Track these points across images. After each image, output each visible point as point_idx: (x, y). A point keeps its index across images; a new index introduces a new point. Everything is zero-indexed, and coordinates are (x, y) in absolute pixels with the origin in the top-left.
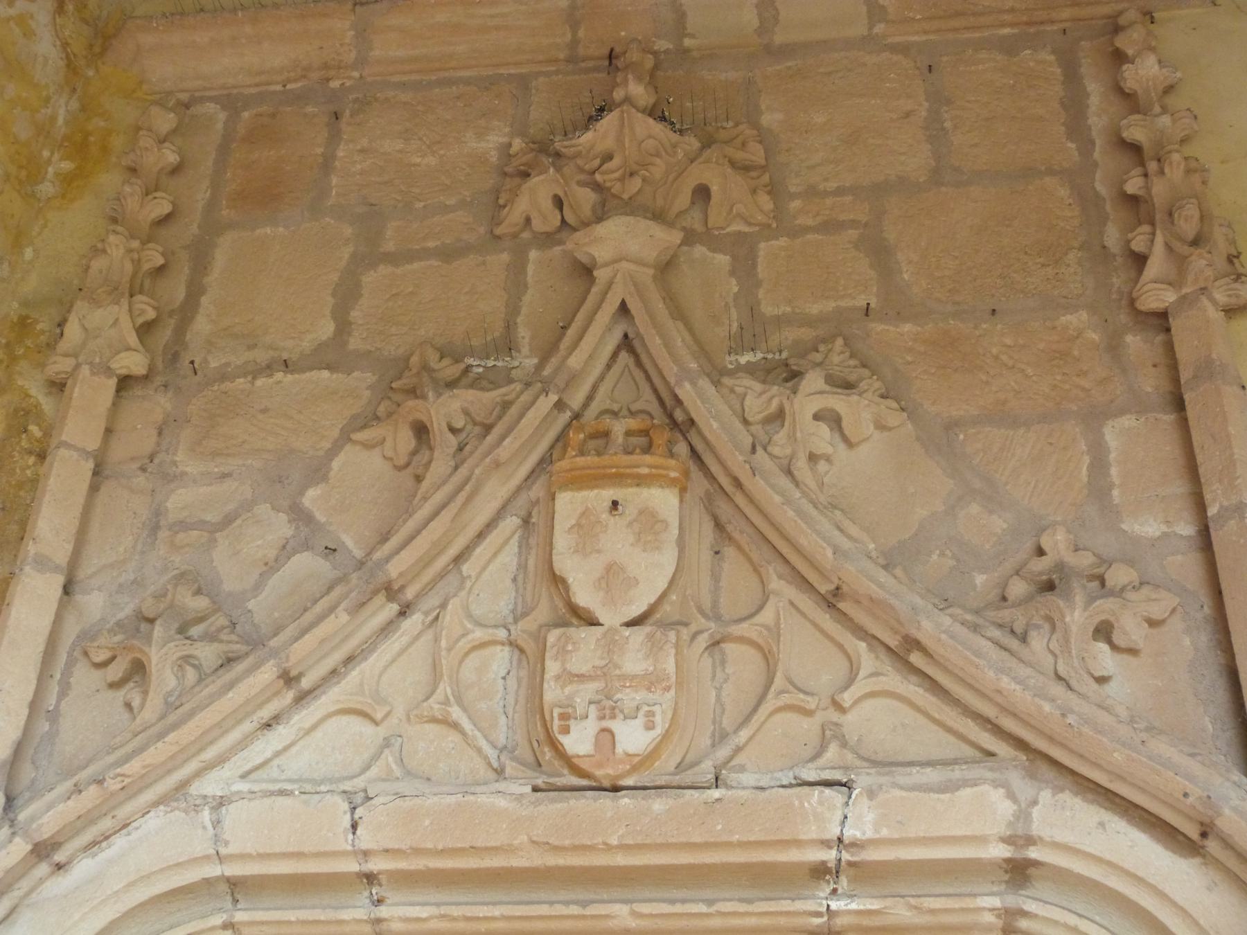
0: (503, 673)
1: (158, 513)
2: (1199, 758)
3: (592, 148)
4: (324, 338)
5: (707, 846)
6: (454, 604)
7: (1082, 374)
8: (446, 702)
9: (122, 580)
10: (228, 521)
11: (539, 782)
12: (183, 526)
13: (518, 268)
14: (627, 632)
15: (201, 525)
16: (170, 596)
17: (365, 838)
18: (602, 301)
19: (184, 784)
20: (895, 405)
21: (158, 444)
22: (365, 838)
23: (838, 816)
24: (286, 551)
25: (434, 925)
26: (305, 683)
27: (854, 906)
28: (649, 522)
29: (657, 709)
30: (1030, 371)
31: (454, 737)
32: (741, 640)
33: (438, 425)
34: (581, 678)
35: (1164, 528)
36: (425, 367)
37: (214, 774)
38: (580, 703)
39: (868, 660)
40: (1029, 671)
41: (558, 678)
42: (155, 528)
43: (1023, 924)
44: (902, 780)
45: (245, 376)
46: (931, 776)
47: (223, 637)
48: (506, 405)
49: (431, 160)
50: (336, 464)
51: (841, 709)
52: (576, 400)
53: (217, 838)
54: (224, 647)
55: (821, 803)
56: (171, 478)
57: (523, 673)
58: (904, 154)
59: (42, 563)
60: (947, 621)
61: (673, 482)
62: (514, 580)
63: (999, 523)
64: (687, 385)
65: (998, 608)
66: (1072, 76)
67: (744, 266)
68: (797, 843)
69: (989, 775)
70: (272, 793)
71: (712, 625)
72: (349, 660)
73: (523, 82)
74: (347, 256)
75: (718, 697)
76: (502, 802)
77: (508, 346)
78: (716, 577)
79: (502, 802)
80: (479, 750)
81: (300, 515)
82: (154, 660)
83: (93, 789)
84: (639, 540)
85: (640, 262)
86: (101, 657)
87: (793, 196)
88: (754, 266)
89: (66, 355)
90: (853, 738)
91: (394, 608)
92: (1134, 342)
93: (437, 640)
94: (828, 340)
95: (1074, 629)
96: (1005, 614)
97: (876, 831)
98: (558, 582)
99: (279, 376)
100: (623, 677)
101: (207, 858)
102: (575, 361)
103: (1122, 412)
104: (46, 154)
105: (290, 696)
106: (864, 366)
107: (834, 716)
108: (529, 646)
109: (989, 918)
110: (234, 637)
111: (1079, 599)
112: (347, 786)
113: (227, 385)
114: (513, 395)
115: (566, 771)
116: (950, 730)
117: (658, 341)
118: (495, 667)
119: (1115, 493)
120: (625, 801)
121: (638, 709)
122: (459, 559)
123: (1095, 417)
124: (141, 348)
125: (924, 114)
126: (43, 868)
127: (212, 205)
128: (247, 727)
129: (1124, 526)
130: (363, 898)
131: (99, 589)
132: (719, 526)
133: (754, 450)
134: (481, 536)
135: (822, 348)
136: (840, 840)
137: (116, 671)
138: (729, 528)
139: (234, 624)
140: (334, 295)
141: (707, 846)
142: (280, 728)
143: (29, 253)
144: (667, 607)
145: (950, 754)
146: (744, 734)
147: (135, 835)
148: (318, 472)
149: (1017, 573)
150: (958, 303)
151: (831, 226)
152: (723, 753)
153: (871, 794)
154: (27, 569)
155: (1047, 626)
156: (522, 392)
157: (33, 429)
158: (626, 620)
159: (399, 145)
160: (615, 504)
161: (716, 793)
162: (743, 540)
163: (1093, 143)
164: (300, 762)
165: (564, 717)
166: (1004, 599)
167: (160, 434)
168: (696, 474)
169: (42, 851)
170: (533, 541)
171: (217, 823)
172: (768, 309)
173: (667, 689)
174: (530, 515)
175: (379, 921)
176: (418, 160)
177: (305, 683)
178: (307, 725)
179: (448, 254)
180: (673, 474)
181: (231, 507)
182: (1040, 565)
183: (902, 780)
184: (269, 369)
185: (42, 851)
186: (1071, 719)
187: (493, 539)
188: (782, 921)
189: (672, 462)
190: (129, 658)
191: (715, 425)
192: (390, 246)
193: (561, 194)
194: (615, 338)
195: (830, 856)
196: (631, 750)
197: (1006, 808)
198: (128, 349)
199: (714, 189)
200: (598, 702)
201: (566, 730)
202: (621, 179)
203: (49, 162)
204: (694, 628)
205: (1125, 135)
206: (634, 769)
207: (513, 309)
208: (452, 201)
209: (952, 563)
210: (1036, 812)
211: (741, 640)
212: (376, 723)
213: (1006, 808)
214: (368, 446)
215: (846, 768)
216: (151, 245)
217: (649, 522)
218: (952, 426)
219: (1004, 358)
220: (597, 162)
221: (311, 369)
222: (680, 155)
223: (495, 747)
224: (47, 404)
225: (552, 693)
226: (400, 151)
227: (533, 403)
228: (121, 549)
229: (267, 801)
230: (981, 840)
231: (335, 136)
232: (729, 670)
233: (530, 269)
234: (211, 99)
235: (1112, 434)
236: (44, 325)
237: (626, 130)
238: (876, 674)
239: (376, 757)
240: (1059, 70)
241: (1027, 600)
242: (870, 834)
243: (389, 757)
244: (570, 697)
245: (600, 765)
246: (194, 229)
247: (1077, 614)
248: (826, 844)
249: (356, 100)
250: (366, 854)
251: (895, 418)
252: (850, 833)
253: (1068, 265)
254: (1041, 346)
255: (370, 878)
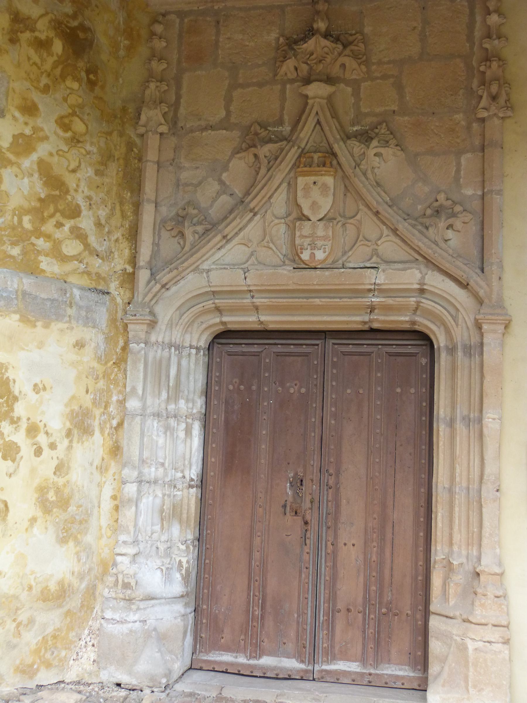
0: (284, 232)
1: (178, 180)
2: (468, 265)
3: (306, 50)
4: (223, 117)
5: (339, 285)
6: (269, 212)
7: (458, 137)
8: (268, 242)
9: (171, 203)
10: (200, 183)
11: (295, 266)
12: (186, 185)
13: (283, 91)
14: (319, 223)
15: (191, 184)
16: (186, 210)
17: (249, 281)
18: (310, 112)
19: (198, 266)
20: (399, 148)
21: (175, 156)
22: (249, 281)
23: (375, 277)
24: (219, 194)
25: (268, 303)
26: (229, 237)
27: (378, 300)
28: (325, 187)
29: (327, 247)
30: (442, 136)
31: (270, 252)
32: (351, 224)
33: (261, 156)
34: (306, 237)
35: (473, 192)
36: (256, 134)
37: (206, 263)
38: (306, 244)
39: (386, 232)
40: (427, 240)
41: (299, 237)
42: (178, 186)
43: (421, 304)
44: (392, 267)
45: (199, 131)
46: (400, 266)
47: (203, 223)
48: (282, 150)
49: (252, 44)
50: (230, 165)
51: (377, 245)
52: (303, 146)
53: (208, 281)
54: (204, 226)
55: (370, 273)
56: (180, 168)
57: (289, 232)
58: (411, 46)
59: (149, 201)
60: (406, 224)
61: (332, 175)
62: (286, 203)
63: (427, 189)
64: (336, 145)
65: (423, 218)
66: (472, 14)
67: (356, 93)
68: (364, 284)
69: (416, 266)
70: (222, 268)
71: (343, 219)
72: (241, 230)
73: (282, 8)
74: (227, 84)
75: (344, 240)
76: (285, 272)
77: (281, 122)
78: (344, 203)
79: (285, 272)
80: (278, 256)
81: (222, 182)
82: (186, 233)
83: (175, 271)
84: (322, 193)
85: (322, 98)
86: (169, 228)
87: (374, 64)
88: (360, 93)
89: (143, 126)
90: (380, 253)
91: (252, 214)
92: (475, 125)
93: (264, 222)
94: (380, 123)
95: (440, 228)
96: (425, 220)
97: (385, 281)
98: (299, 206)
99: (210, 131)
100: (317, 237)
101: (206, 286)
102: (302, 135)
103: (468, 152)
104: (119, 38)
105: (225, 241)
106: (392, 133)
107: (376, 247)
108: (291, 225)
109: (413, 303)
110: (206, 223)
111: (443, 219)
112: (242, 266)
113: (194, 134)
114: (284, 146)
115: (302, 263)
116: (407, 252)
117: (328, 128)
118: (281, 230)
119: (461, 180)
120: (318, 272)
121: (321, 247)
122: (270, 198)
123: (459, 154)
124: (166, 124)
125: (420, 29)
126: (164, 290)
127: (179, 62)
128: (213, 250)
129: (462, 191)
130: (248, 296)
131: (164, 205)
132: (345, 186)
133: (355, 168)
134: (276, 190)
135: (379, 127)
136: (375, 283)
137: (174, 233)
138: (349, 188)
139: (206, 218)
140: (224, 100)
141: (339, 285)
142: (222, 249)
143: (121, 80)
144: (330, 214)
145: (407, 257)
146: (350, 253)
147: (186, 280)
148: (225, 168)
149: (429, 207)
150: (423, 109)
151: (385, 77)
152: (344, 258)
153: (384, 271)
154: (145, 203)
155: (434, 226)
156: (286, 145)
157: (135, 149)
158: (318, 219)
159: (241, 37)
160: (315, 183)
161: (343, 270)
162: (353, 193)
163: (474, 44)
164: (228, 259)
165: (301, 249)
166: (425, 215)
167: (175, 152)
168: (339, 170)
169: (163, 286)
170: (291, 190)
171: (208, 277)
172: (364, 110)
173: (330, 240)
174: (290, 182)
175: (253, 302)
176: (248, 44)
177: (229, 237)
178: (229, 248)
179: (260, 85)
180: (332, 173)
181: (200, 178)
182: (436, 204)
183: (392, 267)
184: (205, 129)
185: (163, 286)
186: (436, 255)
187: (280, 190)
188: (359, 303)
189: (332, 169)
190: (178, 230)
191: (344, 159)
192: (241, 81)
193: (297, 66)
194: (316, 120)
195: (372, 287)
196: (319, 259)
197: (419, 276)
198: (161, 124)
199: (347, 65)
200: (310, 245)
201: (302, 253)
202: (316, 63)
203: (121, 42)
204: (337, 220)
205: (483, 46)
206: (320, 264)
207: (282, 108)
208: (260, 63)
209: (412, 201)
210: (426, 277)
211: (351, 224)
212: (249, 247)
213: (419, 276)
214: (240, 159)
215: (377, 263)
216: (163, 83)
217: (325, 187)
218: (417, 155)
219: (435, 130)
220: (308, 56)
221: (220, 129)
222: (336, 53)
223: (282, 255)
224: (138, 141)
225: (298, 241)
226: (242, 39)
227: (290, 150)
228: (169, 192)
229: (221, 271)
230: (412, 284)
231: (218, 34)
232: (347, 232)
233: (288, 91)
234: (173, 13)
235: (463, 160)
236: (131, 110)
237: (318, 45)
238: (387, 236)
239: (250, 257)
240: (468, 10)
241: (431, 216)
242: (382, 282)
243: (253, 258)
244: (303, 243)
245: (311, 263)
246: (175, 71)
247: (442, 224)
248: (371, 284)
249: (224, 15)
250: (249, 286)
251: (400, 153)
252: (378, 281)
253: (459, 95)
254: (447, 126)
255: (250, 291)
